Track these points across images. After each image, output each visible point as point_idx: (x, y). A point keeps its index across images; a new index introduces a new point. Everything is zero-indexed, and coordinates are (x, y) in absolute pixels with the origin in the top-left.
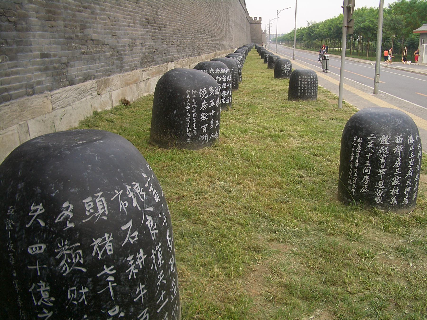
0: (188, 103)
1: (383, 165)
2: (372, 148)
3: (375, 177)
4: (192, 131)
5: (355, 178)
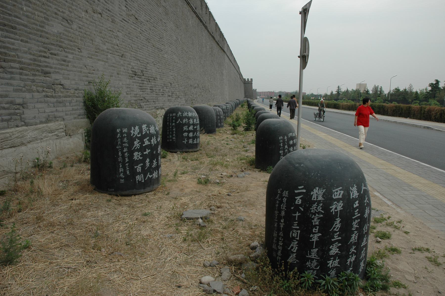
0: (119, 143)
1: (316, 228)
2: (301, 205)
3: (305, 244)
4: (125, 173)
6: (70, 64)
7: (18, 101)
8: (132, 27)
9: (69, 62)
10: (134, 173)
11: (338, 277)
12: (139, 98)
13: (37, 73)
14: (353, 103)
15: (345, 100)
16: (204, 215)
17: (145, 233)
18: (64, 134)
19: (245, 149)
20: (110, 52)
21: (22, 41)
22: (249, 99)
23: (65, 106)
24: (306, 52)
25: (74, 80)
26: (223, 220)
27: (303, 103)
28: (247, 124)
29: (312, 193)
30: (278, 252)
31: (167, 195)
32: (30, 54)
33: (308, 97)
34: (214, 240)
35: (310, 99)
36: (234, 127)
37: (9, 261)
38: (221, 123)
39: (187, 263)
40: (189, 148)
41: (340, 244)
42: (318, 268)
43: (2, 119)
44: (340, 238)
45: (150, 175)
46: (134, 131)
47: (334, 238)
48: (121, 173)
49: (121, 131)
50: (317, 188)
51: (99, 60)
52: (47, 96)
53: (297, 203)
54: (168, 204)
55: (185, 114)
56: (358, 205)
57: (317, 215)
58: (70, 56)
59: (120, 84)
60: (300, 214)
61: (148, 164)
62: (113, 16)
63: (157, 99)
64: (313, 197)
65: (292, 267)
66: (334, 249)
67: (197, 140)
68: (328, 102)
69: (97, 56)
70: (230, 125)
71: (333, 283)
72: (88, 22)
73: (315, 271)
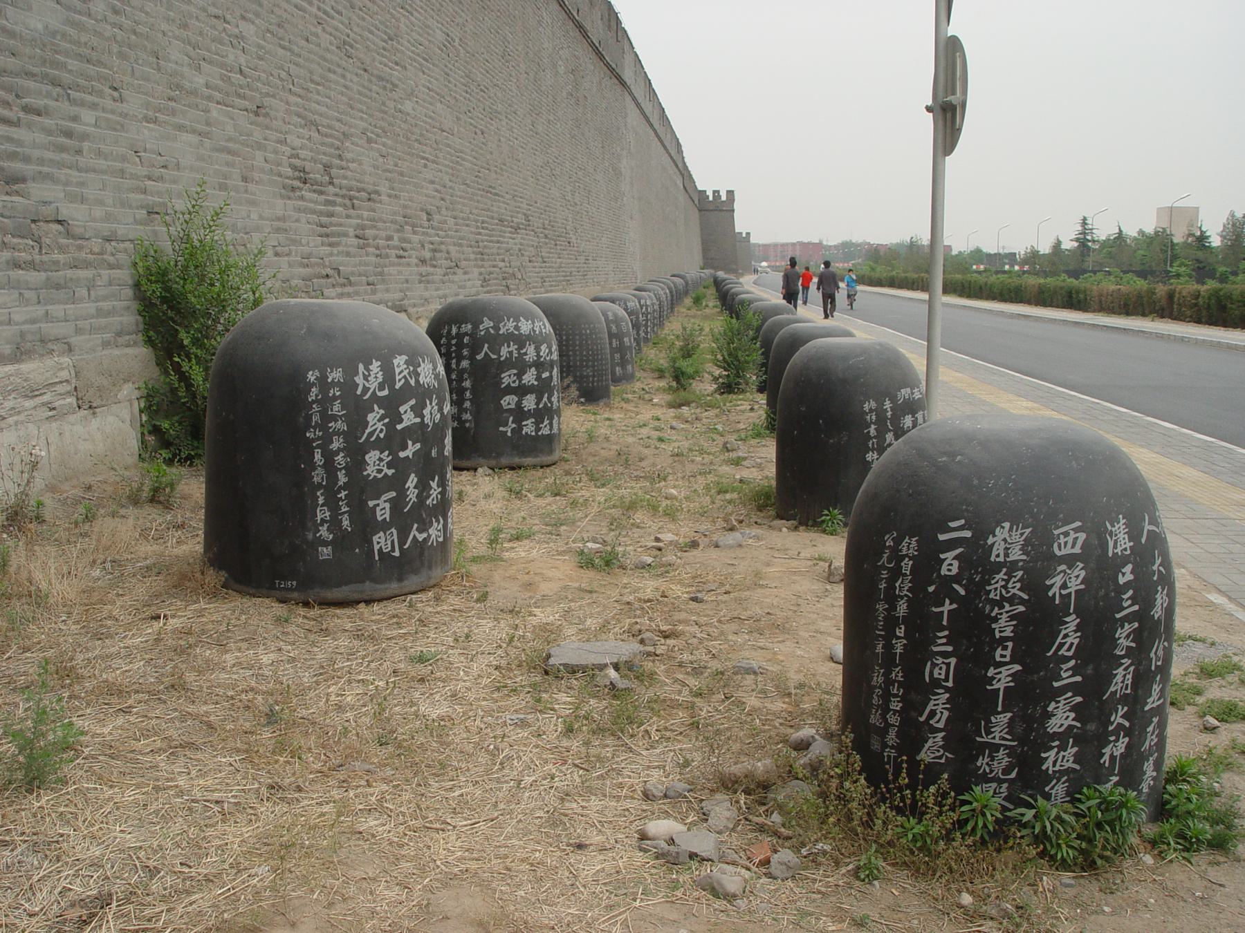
0: (316, 418)
1: (1005, 648)
2: (956, 579)
3: (972, 701)
4: (335, 523)
5: (896, 705)
6: (86, 145)
9: (84, 137)
10: (366, 525)
11: (1073, 801)
12: (317, 270)
14: (1141, 284)
15: (1109, 273)
16: (624, 658)
17: (436, 711)
18: (71, 400)
19: (733, 455)
22: (721, 274)
23: (74, 300)
24: (954, 93)
25: (101, 203)
26: (688, 673)
27: (946, 291)
28: (726, 365)
29: (990, 541)
30: (887, 732)
31: (478, 601)
33: (958, 264)
34: (666, 729)
35: (967, 270)
36: (680, 378)
37: (34, 775)
38: (623, 364)
39: (588, 790)
40: (523, 454)
41: (1079, 699)
42: (1013, 775)
44: (1079, 679)
45: (420, 531)
46: (366, 378)
47: (1060, 678)
48: (322, 525)
49: (322, 380)
50: (1007, 525)
51: (180, 128)
52: (17, 266)
53: (944, 572)
54: (488, 630)
55: (508, 326)
56: (1131, 577)
57: (1007, 607)
58: (88, 116)
59: (254, 216)
60: (955, 606)
61: (412, 495)
63: (381, 274)
64: (994, 553)
65: (932, 773)
66: (1059, 713)
67: (551, 424)
68: (1042, 281)
69: (173, 113)
70: (661, 374)
71: (1059, 818)
73: (1005, 785)
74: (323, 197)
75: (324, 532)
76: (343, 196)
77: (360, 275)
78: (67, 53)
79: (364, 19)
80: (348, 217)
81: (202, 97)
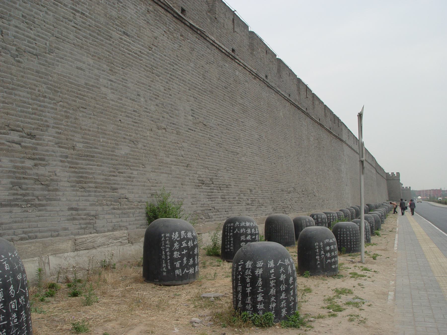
0: (163, 244)
2: (240, 271)
4: (167, 267)
6: (134, 180)
7: (93, 213)
8: (199, 135)
9: (134, 178)
10: (174, 268)
12: (206, 208)
13: (107, 190)
18: (127, 241)
20: (174, 163)
21: (98, 165)
24: (363, 157)
25: (138, 193)
32: (103, 175)
43: (81, 227)
45: (187, 270)
46: (174, 236)
49: (165, 236)
52: (114, 209)
55: (243, 224)
58: (135, 172)
59: (185, 194)
62: (178, 128)
63: (231, 208)
66: (259, 297)
69: (160, 169)
72: (152, 140)
74: (210, 188)
75: (164, 269)
76: (217, 187)
77: (222, 209)
78: (130, 158)
79: (226, 136)
80: (218, 192)
81: (169, 164)
